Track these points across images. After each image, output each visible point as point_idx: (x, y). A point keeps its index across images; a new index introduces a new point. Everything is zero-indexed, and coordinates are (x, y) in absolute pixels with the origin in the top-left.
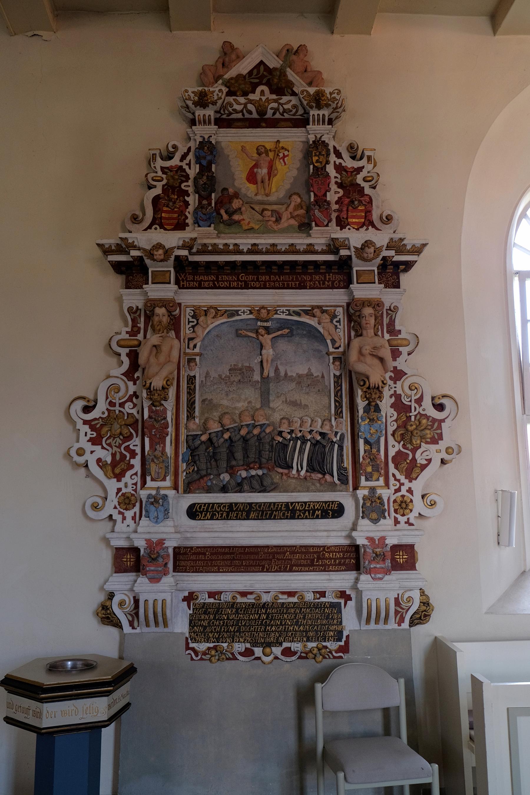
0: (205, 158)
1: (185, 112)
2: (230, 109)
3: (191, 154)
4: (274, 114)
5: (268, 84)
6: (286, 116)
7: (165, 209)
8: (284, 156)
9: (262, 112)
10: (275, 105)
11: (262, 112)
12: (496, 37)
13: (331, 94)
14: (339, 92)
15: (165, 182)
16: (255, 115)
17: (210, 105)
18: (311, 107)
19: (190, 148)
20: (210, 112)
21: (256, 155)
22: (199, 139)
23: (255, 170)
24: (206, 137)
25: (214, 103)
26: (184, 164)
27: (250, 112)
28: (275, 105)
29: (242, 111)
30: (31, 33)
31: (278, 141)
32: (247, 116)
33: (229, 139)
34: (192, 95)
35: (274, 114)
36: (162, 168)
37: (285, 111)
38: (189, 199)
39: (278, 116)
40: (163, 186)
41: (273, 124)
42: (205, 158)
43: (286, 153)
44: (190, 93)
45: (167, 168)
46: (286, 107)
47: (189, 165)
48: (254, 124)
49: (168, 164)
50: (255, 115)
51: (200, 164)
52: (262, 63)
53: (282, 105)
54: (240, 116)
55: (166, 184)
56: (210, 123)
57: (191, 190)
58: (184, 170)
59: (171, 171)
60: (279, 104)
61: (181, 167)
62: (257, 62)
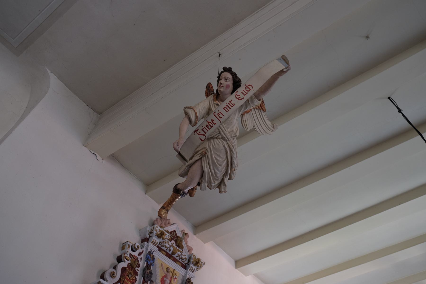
0: (150, 261)
1: (147, 233)
2: (164, 244)
3: (143, 254)
4: (177, 257)
5: (176, 241)
6: (180, 260)
7: (127, 277)
8: (175, 279)
9: (173, 253)
10: (179, 253)
11: (173, 253)
12: (236, 270)
13: (202, 263)
14: (204, 264)
15: (129, 262)
16: (170, 253)
17: (161, 239)
18: (192, 263)
19: (143, 251)
20: (158, 241)
21: (166, 272)
22: (149, 250)
23: (165, 279)
24: (152, 251)
25: (163, 239)
26: (139, 257)
27: (170, 250)
28: (179, 253)
29: (167, 248)
30: (93, 152)
31: (174, 270)
32: (168, 251)
33: (158, 257)
34: (158, 230)
35: (177, 257)
36: (130, 254)
37: (182, 258)
38: (138, 278)
39: (177, 258)
40: (128, 264)
41: (175, 260)
42: (150, 261)
43: (176, 277)
44: (158, 229)
45: (132, 255)
46: (183, 257)
47: (141, 259)
48: (169, 256)
49: (133, 253)
50: (170, 253)
51: (147, 263)
52: (175, 231)
53: (182, 255)
54: (165, 249)
55: (130, 264)
56: (155, 245)
57: (139, 273)
58: (138, 261)
59: (133, 258)
60: (181, 254)
61: (138, 258)
62: (174, 230)
